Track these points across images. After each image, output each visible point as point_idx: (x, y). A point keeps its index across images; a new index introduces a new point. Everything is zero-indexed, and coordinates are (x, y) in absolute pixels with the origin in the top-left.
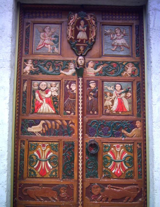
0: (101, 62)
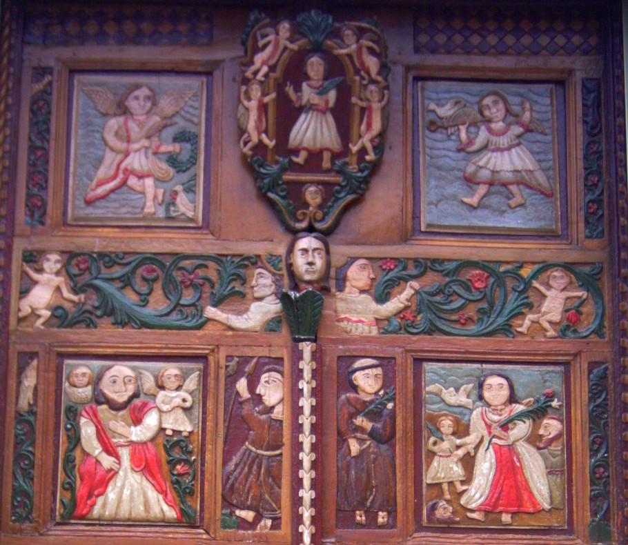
0: (411, 265)
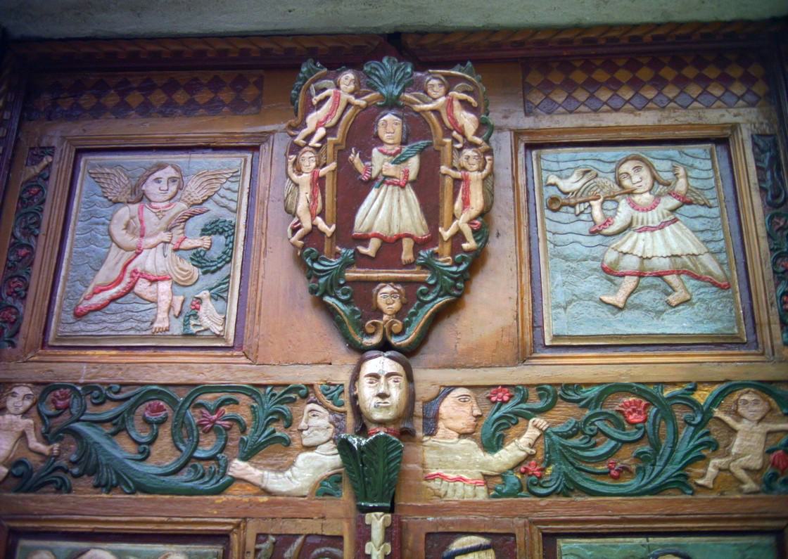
0: (533, 394)
